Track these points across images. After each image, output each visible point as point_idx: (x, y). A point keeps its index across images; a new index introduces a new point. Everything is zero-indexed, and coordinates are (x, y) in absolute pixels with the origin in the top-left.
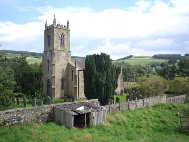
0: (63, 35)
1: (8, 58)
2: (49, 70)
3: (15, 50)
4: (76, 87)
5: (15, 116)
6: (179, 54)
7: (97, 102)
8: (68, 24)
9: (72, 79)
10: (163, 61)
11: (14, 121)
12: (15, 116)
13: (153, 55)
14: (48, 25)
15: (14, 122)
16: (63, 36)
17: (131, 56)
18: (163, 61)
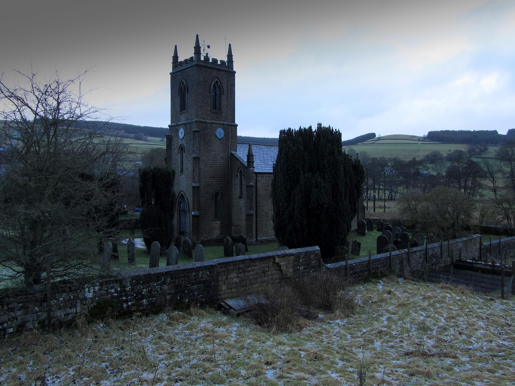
0: (219, 83)
1: (425, 172)
2: (185, 170)
3: (130, 124)
4: (252, 215)
5: (128, 289)
6: (508, 130)
7: (316, 255)
8: (230, 56)
9: (239, 194)
10: (453, 148)
11: (127, 301)
12: (128, 289)
13: (426, 134)
14: (181, 59)
15: (125, 305)
16: (219, 87)
17: (373, 135)
18: (453, 148)
